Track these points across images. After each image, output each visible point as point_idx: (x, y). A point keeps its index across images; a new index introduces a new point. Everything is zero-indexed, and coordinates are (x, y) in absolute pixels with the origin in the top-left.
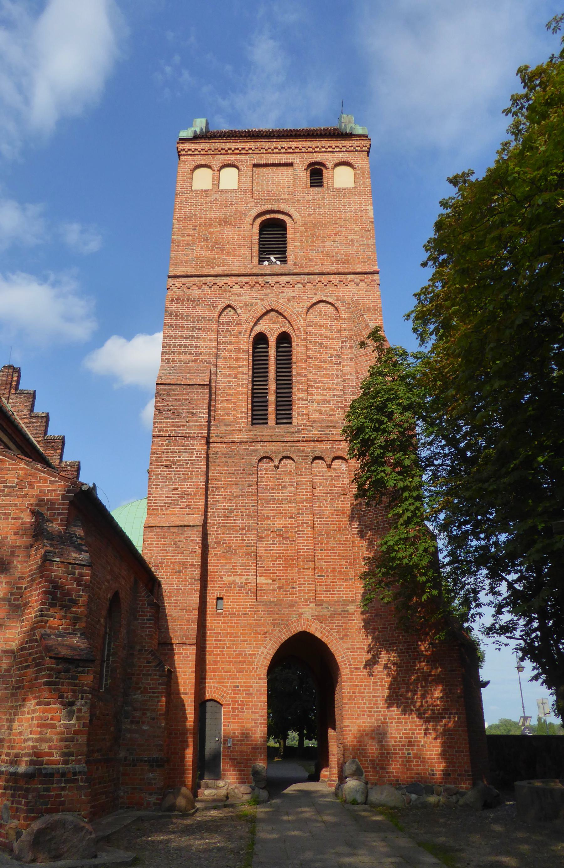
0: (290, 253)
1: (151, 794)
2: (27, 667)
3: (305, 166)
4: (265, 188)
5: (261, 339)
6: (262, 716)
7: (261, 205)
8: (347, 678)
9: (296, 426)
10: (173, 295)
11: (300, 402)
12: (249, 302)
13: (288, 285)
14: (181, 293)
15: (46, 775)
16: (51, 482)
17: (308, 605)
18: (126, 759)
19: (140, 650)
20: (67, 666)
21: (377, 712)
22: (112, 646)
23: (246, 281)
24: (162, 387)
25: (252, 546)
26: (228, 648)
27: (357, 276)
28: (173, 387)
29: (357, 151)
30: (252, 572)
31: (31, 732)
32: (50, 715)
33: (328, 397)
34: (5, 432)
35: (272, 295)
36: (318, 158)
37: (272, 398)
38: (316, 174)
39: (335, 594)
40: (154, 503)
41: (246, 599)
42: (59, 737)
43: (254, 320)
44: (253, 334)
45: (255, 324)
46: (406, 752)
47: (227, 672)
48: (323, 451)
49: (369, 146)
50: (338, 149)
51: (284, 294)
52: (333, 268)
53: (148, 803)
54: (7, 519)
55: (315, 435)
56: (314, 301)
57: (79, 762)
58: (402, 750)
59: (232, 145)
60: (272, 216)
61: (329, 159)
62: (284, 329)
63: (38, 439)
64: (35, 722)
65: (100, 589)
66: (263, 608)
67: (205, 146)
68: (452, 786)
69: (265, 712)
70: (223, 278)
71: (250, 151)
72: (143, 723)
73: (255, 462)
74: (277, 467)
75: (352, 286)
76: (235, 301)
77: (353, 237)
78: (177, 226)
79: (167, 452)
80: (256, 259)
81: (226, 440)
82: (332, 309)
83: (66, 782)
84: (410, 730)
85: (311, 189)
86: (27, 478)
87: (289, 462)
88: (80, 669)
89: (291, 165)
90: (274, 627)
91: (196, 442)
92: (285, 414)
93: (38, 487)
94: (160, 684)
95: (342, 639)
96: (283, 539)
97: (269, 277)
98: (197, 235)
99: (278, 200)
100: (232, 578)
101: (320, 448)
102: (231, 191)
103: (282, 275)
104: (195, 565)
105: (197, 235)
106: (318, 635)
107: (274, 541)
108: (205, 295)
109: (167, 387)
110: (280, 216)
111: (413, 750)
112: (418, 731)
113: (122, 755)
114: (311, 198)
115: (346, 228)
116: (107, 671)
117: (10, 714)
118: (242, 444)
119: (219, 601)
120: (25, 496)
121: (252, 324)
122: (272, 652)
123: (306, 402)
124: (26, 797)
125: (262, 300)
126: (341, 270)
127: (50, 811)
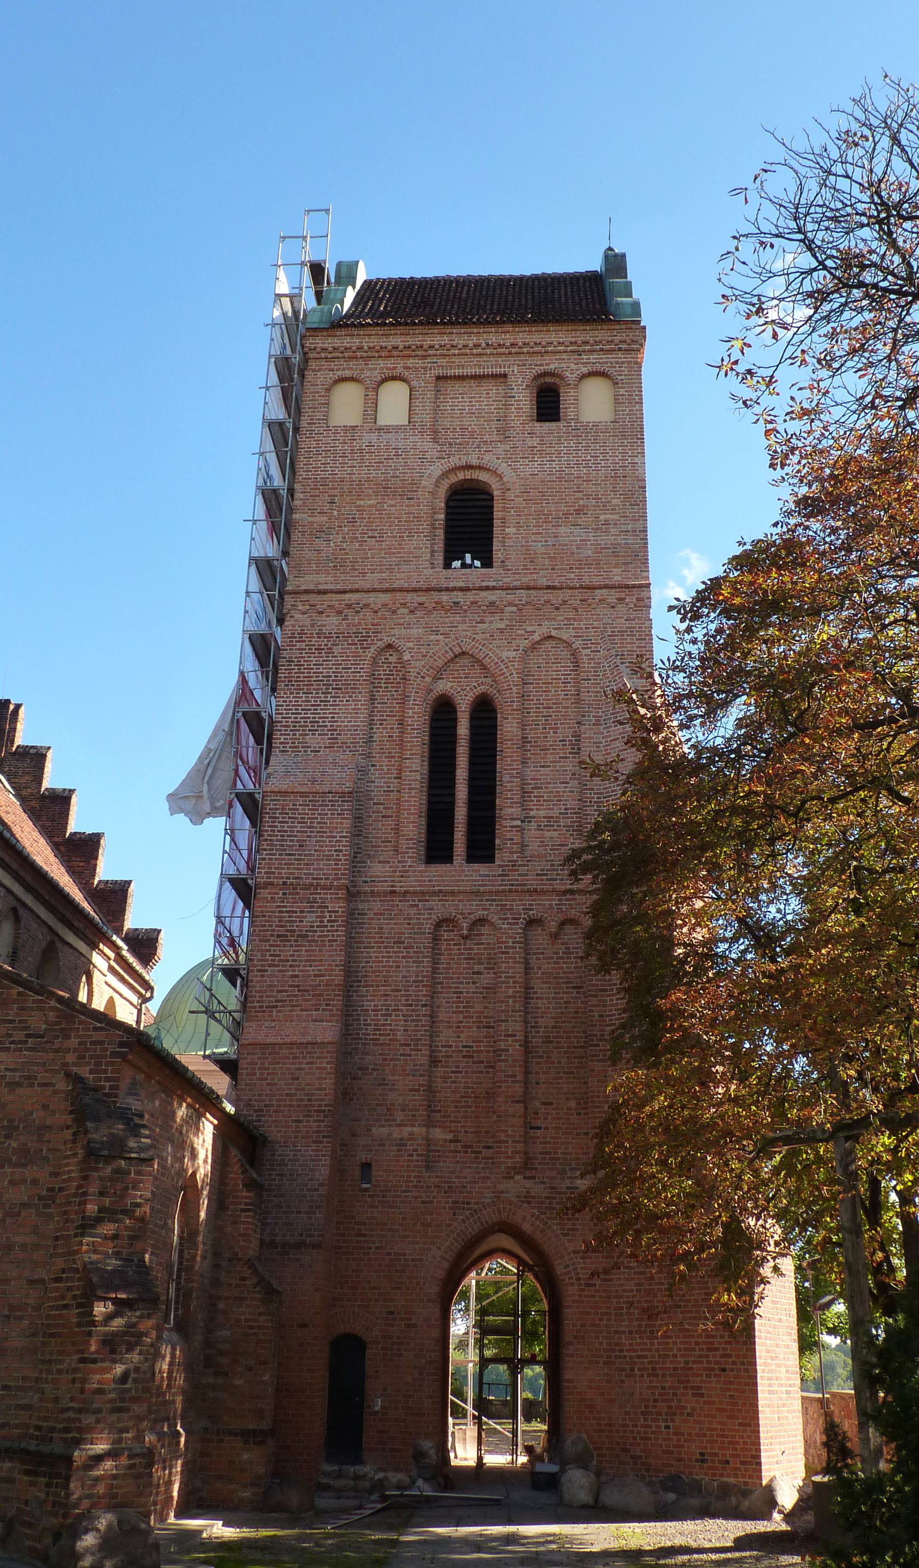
0: (498, 554)
2: (65, 1307)
5: (443, 712)
8: (574, 1301)
10: (294, 626)
12: (423, 643)
14: (308, 622)
16: (96, 1029)
17: (513, 1178)
19: (230, 1260)
21: (620, 1357)
23: (422, 599)
25: (421, 1075)
26: (377, 1248)
29: (620, 349)
31: (72, 1399)
33: (555, 812)
34: (7, 868)
35: (464, 627)
37: (461, 813)
39: (558, 1159)
40: (258, 1002)
41: (408, 1166)
44: (433, 695)
45: (436, 679)
46: (663, 1425)
47: (375, 1288)
54: (32, 1085)
56: (536, 637)
61: (570, 368)
70: (381, 595)
78: (301, 496)
79: (280, 912)
80: (440, 558)
84: (670, 1388)
85: (538, 424)
86: (60, 1023)
87: (485, 930)
89: (505, 376)
90: (454, 1214)
92: (482, 849)
94: (260, 1314)
95: (567, 1235)
96: (474, 1062)
98: (335, 513)
102: (397, 428)
104: (324, 1111)
105: (335, 513)
107: (458, 1067)
111: (673, 1421)
112: (682, 1390)
114: (535, 442)
117: (41, 1372)
126: (586, 580)
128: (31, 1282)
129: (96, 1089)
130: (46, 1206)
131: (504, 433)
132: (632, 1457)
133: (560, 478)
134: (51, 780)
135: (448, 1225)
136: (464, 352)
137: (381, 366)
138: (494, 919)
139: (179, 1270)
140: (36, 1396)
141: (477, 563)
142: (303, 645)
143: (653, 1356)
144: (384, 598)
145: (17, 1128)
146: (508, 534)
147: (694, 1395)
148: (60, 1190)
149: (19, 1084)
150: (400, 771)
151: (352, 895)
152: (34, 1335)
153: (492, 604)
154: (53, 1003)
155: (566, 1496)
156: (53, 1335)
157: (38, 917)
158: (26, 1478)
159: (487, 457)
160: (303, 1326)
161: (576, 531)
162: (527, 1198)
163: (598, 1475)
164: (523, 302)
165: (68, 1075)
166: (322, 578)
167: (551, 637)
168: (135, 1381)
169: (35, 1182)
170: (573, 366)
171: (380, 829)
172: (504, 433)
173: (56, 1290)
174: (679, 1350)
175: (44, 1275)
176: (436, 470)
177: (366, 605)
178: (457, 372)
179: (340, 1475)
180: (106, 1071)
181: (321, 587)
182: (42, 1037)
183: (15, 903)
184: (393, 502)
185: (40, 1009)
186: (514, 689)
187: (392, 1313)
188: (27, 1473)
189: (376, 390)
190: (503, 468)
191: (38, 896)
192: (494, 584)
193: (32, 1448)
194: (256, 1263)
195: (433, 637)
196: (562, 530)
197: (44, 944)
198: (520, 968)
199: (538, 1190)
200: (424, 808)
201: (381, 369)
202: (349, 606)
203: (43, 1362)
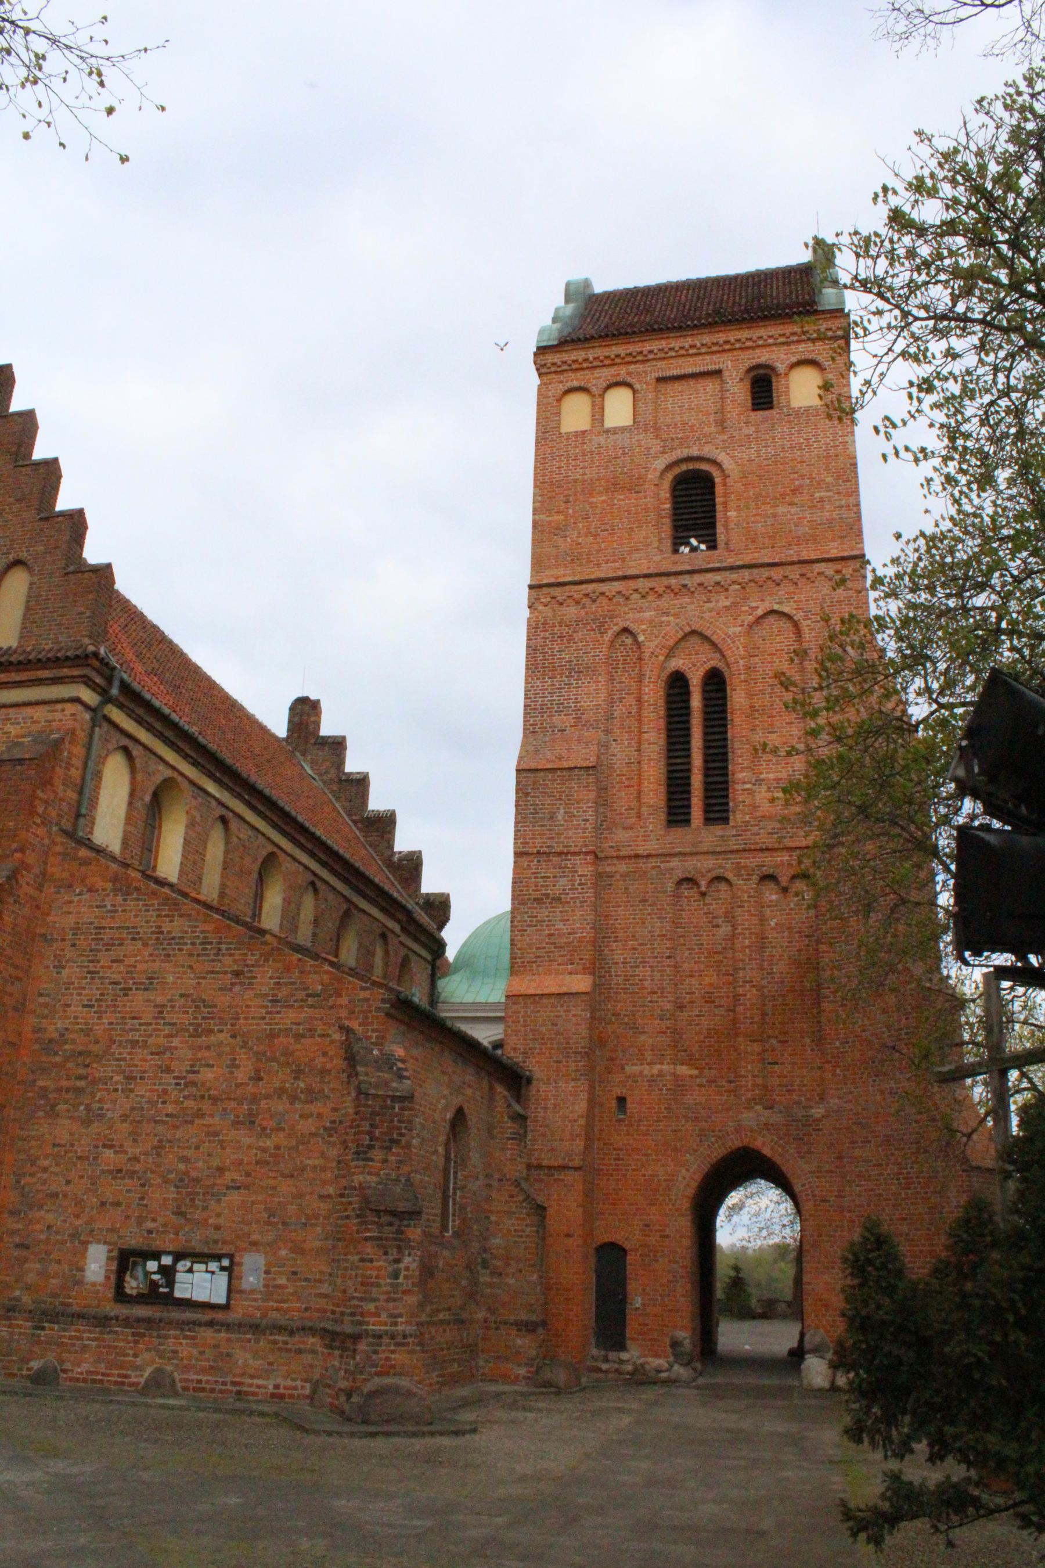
0: (721, 538)
2: (347, 1217)
5: (677, 682)
7: (672, 449)
12: (656, 622)
13: (718, 588)
15: (374, 1336)
19: (500, 1180)
27: (830, 564)
35: (693, 607)
36: (763, 356)
37: (697, 780)
42: (385, 1297)
43: (665, 651)
44: (668, 672)
45: (668, 657)
48: (777, 866)
50: (795, 338)
53: (517, 1377)
54: (313, 1036)
55: (764, 839)
56: (760, 612)
59: (620, 350)
60: (691, 466)
61: (779, 358)
62: (708, 666)
65: (434, 1111)
67: (579, 355)
69: (688, 1262)
71: (651, 356)
72: (507, 1275)
73: (670, 886)
74: (703, 894)
76: (635, 621)
80: (668, 544)
82: (787, 625)
83: (397, 1344)
85: (752, 414)
87: (723, 886)
88: (405, 1223)
89: (719, 372)
91: (578, 860)
92: (718, 811)
97: (687, 576)
100: (636, 1069)
101: (770, 862)
102: (623, 429)
106: (767, 1151)
110: (704, 467)
115: (811, 478)
120: (332, 1007)
123: (749, 786)
126: (805, 555)
130: (330, 1136)
131: (722, 425)
133: (776, 462)
134: (352, 766)
137: (606, 374)
138: (730, 876)
139: (454, 1189)
141: (703, 547)
144: (618, 586)
146: (730, 515)
149: (303, 1036)
150: (639, 743)
152: (326, 1239)
153: (718, 583)
154: (326, 967)
157: (334, 889)
160: (568, 1236)
161: (794, 510)
165: (341, 1028)
166: (561, 571)
168: (406, 1277)
169: (320, 1116)
170: (783, 356)
171: (623, 799)
172: (722, 425)
175: (331, 1190)
176: (660, 464)
177: (602, 594)
180: (372, 1024)
181: (561, 580)
182: (319, 996)
183: (312, 878)
185: (315, 973)
187: (647, 1226)
188: (326, 1346)
189: (602, 396)
191: (333, 871)
195: (664, 619)
196: (781, 510)
197: (341, 913)
198: (755, 920)
199: (776, 1118)
200: (663, 778)
202: (587, 595)
203: (333, 1260)
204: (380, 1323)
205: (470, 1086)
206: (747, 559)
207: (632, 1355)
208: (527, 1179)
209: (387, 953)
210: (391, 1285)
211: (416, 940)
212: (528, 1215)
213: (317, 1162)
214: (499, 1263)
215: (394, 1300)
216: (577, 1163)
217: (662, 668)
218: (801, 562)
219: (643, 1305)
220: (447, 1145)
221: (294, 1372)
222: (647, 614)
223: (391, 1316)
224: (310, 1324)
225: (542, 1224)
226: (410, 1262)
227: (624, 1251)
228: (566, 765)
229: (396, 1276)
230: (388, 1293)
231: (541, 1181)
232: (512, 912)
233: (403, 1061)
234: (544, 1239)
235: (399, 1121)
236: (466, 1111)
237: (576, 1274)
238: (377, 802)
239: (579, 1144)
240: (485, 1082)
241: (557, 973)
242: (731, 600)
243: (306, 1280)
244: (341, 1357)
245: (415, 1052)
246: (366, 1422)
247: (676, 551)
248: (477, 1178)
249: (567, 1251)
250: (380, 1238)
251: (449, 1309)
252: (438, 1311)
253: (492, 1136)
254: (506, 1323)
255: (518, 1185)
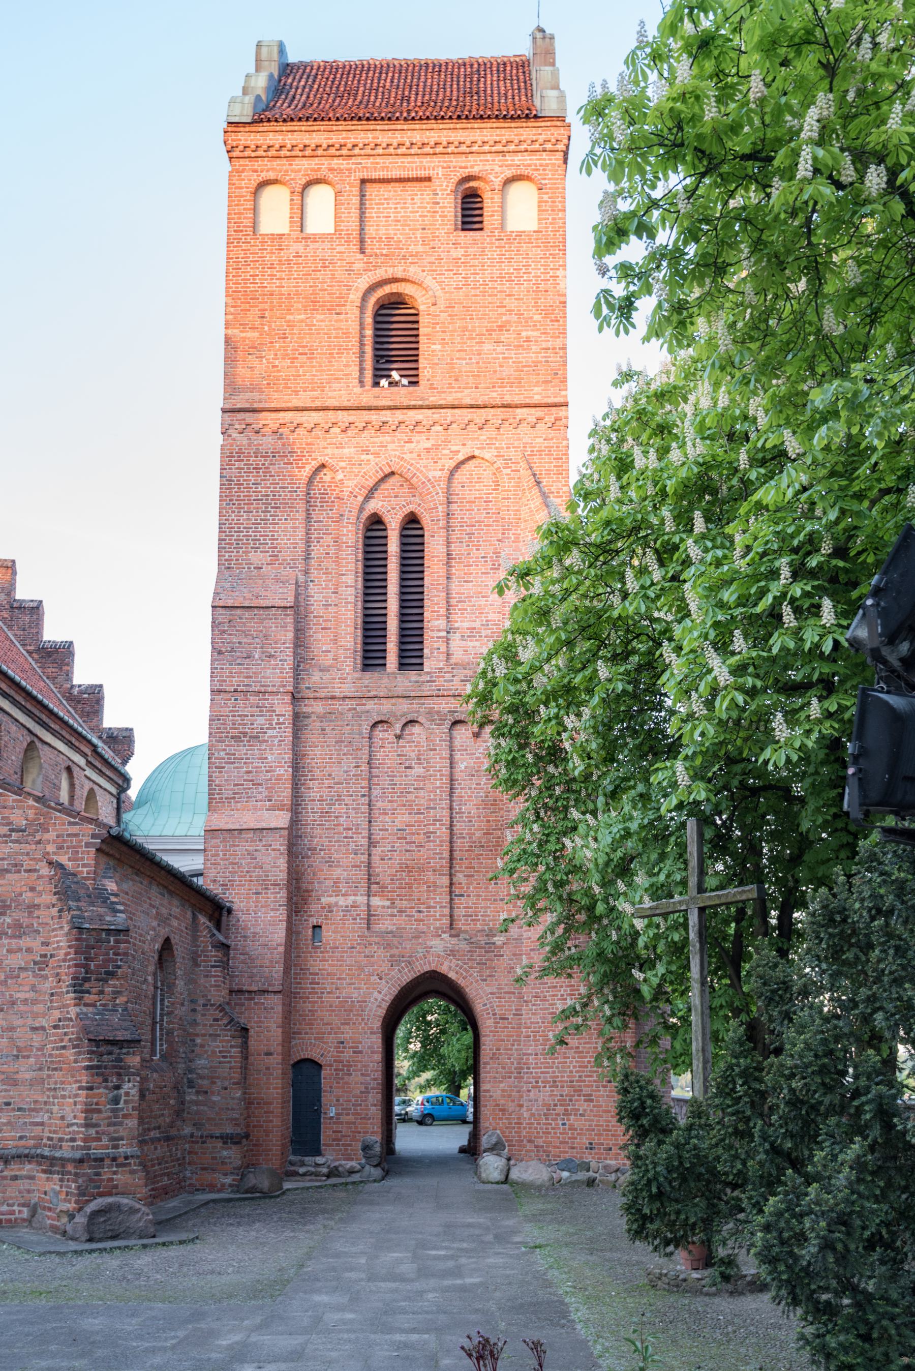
1: (226, 1175)
2: (64, 1047)
3: (451, 186)
4: (382, 231)
5: (375, 525)
6: (375, 1079)
9: (428, 673)
11: (436, 634)
15: (96, 1160)
16: (70, 823)
18: (192, 1136)
19: (204, 1005)
20: (110, 1048)
22: (166, 1003)
23: (351, 419)
24: (221, 611)
27: (533, 410)
28: (239, 612)
30: (363, 890)
31: (75, 1117)
32: (95, 1100)
33: (477, 624)
36: (475, 165)
38: (470, 210)
42: (106, 1121)
43: (364, 492)
45: (368, 498)
49: (566, 141)
51: (412, 446)
52: (494, 394)
53: (223, 1185)
54: (19, 872)
56: (461, 457)
57: (131, 1145)
58: (556, 1120)
61: (491, 170)
62: (406, 510)
63: (28, 648)
64: (79, 1107)
65: (144, 942)
66: (377, 939)
68: (613, 1162)
72: (213, 1093)
73: (365, 728)
75: (524, 428)
77: (530, 333)
81: (323, 695)
83: (118, 1166)
85: (463, 234)
88: (124, 1051)
89: (429, 179)
92: (411, 657)
93: (54, 830)
94: (232, 1047)
97: (388, 412)
98: (266, 328)
99: (404, 258)
100: (333, 900)
102: (323, 237)
103: (408, 408)
105: (266, 328)
106: (452, 975)
108: (283, 445)
109: (228, 612)
113: (187, 1130)
114: (459, 253)
116: (161, 1035)
117: (48, 1097)
118: (347, 701)
119: (317, 930)
120: (39, 842)
121: (360, 499)
122: (389, 998)
124: (75, 1181)
125: (376, 454)
126: (508, 399)
127: (101, 1195)
128: (34, 1029)
129: (74, 875)
132: (536, 1147)
135: (387, 975)
136: (389, 150)
137: (304, 167)
140: (46, 1115)
141: (405, 381)
142: (242, 465)
143: (554, 1072)
144: (316, 417)
145: (9, 907)
147: (585, 1101)
148: (52, 956)
151: (296, 698)
152: (40, 1069)
154: (31, 802)
155: (484, 1175)
156: (55, 1069)
157: (17, 720)
158: (44, 1176)
159: (412, 269)
160: (268, 1054)
162: (453, 953)
163: (509, 1159)
164: (448, 93)
165: (50, 863)
167: (473, 457)
169: (29, 950)
170: (497, 169)
173: (54, 1035)
174: (575, 1067)
178: (382, 174)
179: (303, 1164)
181: (256, 406)
182: (24, 831)
184: (322, 317)
185: (19, 808)
186: (440, 508)
187: (342, 1043)
188: (44, 1172)
189: (302, 194)
190: (429, 281)
192: (420, 403)
193: (46, 1153)
194: (227, 1007)
195: (364, 457)
197: (25, 744)
201: (306, 170)
203: (50, 1089)
204: (103, 1147)
205: (176, 918)
206: (450, 399)
207: (328, 1158)
208: (228, 1003)
209: (72, 786)
210: (113, 1110)
211: (101, 773)
212: (233, 1037)
213: (27, 995)
214: (205, 1082)
215: (115, 1124)
216: (276, 988)
217: (361, 509)
218: (504, 406)
219: (337, 1114)
220: (155, 974)
221: (11, 1198)
222: (346, 451)
223: (113, 1139)
224: (27, 1151)
225: (245, 1046)
226: (130, 1088)
227: (319, 1066)
228: (263, 603)
229: (116, 1100)
230: (110, 1118)
231: (243, 1004)
232: (211, 747)
233: (116, 895)
234: (246, 1058)
235: (115, 954)
236: (173, 942)
237: (274, 1087)
238: (53, 631)
239: (279, 968)
240: (189, 914)
241: (255, 809)
242: (432, 442)
243: (19, 1109)
244: (61, 1180)
245: (125, 886)
246: (90, 1240)
247: (376, 384)
248: (183, 1005)
249: (268, 1069)
250: (98, 1067)
251: (159, 1128)
252: (149, 1130)
253: (196, 964)
254: (212, 1137)
255: (223, 1010)
